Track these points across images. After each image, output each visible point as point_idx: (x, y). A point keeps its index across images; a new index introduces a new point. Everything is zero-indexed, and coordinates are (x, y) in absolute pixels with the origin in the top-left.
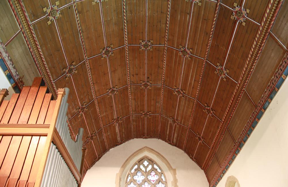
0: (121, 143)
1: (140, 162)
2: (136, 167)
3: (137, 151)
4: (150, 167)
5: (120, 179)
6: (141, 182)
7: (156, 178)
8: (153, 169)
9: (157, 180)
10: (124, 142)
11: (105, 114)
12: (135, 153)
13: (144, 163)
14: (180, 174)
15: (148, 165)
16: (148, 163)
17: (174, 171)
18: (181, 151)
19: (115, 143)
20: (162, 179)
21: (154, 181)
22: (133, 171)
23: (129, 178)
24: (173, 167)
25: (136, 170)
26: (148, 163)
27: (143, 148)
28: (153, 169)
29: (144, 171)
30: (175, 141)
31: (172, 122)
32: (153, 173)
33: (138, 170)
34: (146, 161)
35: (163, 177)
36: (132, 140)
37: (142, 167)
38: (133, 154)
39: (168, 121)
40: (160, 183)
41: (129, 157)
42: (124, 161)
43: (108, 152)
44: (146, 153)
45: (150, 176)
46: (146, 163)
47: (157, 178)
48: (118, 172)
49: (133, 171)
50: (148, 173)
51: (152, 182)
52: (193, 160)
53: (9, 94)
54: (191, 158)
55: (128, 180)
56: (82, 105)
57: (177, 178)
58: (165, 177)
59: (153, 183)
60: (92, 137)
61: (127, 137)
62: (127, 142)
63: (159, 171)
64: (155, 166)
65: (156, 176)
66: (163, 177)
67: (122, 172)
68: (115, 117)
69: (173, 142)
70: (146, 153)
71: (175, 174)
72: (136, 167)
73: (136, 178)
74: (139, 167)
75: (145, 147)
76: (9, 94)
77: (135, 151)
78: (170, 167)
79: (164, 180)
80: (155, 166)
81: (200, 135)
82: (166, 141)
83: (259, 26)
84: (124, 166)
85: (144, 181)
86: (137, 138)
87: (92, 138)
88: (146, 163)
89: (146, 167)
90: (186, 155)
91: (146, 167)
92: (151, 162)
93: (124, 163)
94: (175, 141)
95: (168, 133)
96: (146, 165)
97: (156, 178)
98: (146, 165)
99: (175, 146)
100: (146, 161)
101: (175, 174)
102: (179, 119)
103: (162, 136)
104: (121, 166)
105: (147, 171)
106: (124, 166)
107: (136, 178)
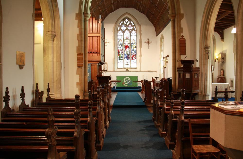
0: (114, 11)
1: (124, 20)
2: (122, 22)
3: (122, 15)
4: (129, 22)
5: (115, 30)
6: (124, 30)
7: (132, 28)
8: (130, 24)
9: (132, 29)
10: (116, 10)
11: (108, 3)
12: (121, 16)
13: (126, 20)
14: (143, 27)
15: (128, 21)
16: (128, 20)
17: (140, 26)
18: (144, 15)
19: (112, 11)
20: (134, 29)
21: (130, 30)
22: (120, 24)
23: (119, 28)
24: (140, 24)
25: (122, 24)
26: (128, 20)
27: (125, 13)
28: (130, 24)
29: (126, 24)
30: (141, 11)
31: (139, 4)
32: (130, 26)
33: (123, 24)
34: (127, 19)
35: (135, 28)
36: (119, 9)
37: (125, 22)
38: (120, 17)
39: (138, 3)
40: (133, 31)
41: (119, 18)
42: (116, 20)
43: (108, 16)
44: (127, 15)
45: (129, 27)
46: (127, 20)
47: (132, 28)
48: (113, 26)
49: (120, 24)
50: (127, 26)
51: (130, 30)
52: (150, 21)
53: (117, 76)
54: (149, 19)
55: (118, 29)
56: (99, 4)
57: (141, 29)
58: (136, 28)
59: (130, 31)
60: (102, 13)
61: (118, 8)
62: (117, 10)
63: (133, 24)
64: (131, 22)
65: (131, 27)
66: (135, 28)
67: (115, 26)
68: (112, 2)
69: (140, 10)
70: (127, 15)
71: (140, 27)
72: (122, 22)
73: (122, 28)
74: (123, 22)
75: (126, 13)
76: (117, 76)
77: (122, 15)
78: (138, 24)
79: (135, 29)
80: (131, 22)
81: (156, 5)
82: (137, 9)
83: (165, 4)
84: (116, 23)
85: (126, 30)
86: (122, 7)
87: (99, 6)
88: (127, 20)
89: (127, 23)
90: (146, 17)
91: (127, 23)
92: (129, 20)
93: (116, 22)
94: (141, 11)
95: (138, 7)
96: (127, 21)
97: (132, 28)
98: (127, 21)
99: (141, 12)
100: (127, 19)
101: (140, 27)
102: (143, 4)
103: (135, 7)
104: (115, 23)
105: (127, 25)
106: (116, 23)
107: (122, 28)
